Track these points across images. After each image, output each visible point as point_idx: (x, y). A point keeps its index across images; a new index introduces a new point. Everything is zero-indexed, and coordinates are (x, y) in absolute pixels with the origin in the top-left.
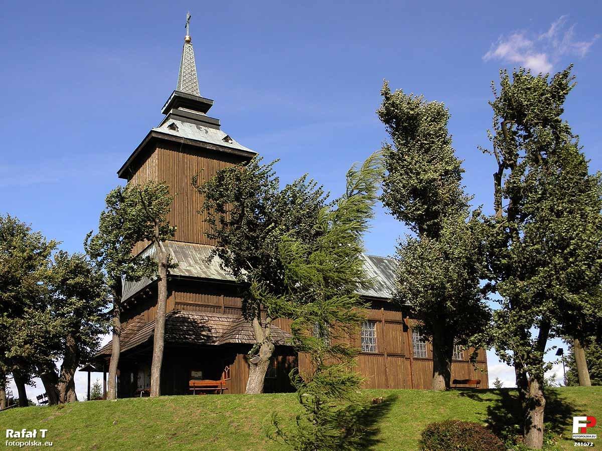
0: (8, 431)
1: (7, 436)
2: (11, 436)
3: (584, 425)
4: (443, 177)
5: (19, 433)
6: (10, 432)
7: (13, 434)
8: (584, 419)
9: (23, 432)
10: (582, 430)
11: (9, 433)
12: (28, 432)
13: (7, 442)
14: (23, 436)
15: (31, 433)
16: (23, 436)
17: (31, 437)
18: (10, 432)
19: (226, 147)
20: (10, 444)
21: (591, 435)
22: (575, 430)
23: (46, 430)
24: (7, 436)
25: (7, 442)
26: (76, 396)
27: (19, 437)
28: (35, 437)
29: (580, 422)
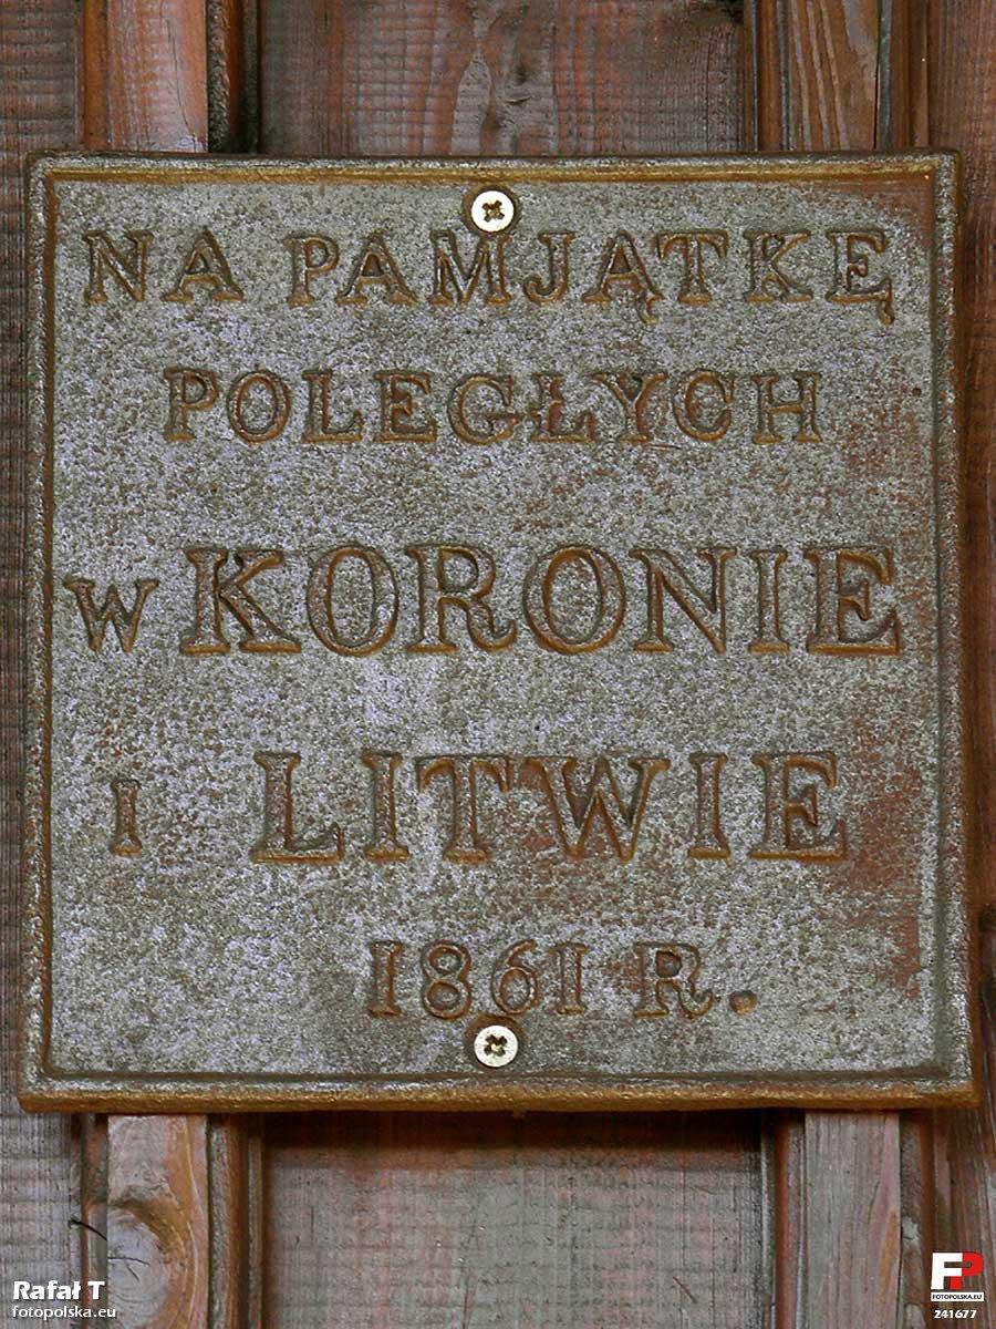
0: (17, 1284)
1: (16, 1297)
2: (25, 1297)
3: (957, 1272)
4: (154, 728)
5: (41, 1289)
6: (22, 1287)
7: (29, 1292)
8: (957, 1257)
9: (51, 1286)
10: (950, 1284)
11: (20, 1289)
12: (61, 1287)
13: (14, 1310)
14: (51, 1297)
15: (67, 1289)
16: (51, 1297)
17: (42, 1297)
18: (22, 1287)
19: (929, 115)
20: (23, 1313)
21: (972, 1294)
22: (937, 1282)
23: (103, 1283)
24: (16, 1297)
25: (14, 1310)
26: (901, 1157)
27: (42, 1297)
28: (76, 1297)
29: (948, 1265)
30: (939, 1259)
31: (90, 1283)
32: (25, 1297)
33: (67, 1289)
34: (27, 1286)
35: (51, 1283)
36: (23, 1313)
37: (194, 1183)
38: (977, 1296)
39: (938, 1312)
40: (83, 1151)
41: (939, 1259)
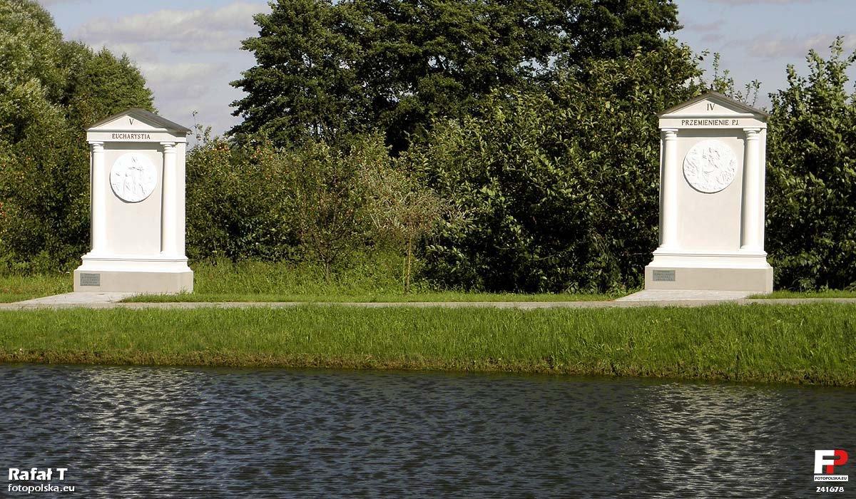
0: (11, 470)
1: (10, 478)
3: (831, 462)
5: (27, 474)
6: (14, 472)
7: (19, 475)
8: (831, 453)
10: (826, 470)
11: (13, 473)
12: (39, 472)
13: (9, 487)
14: (33, 478)
15: (43, 473)
16: (33, 478)
18: (14, 472)
20: (15, 489)
21: (841, 476)
22: (818, 469)
25: (9, 487)
27: (27, 478)
28: (49, 478)
29: (825, 458)
30: (819, 454)
31: (58, 470)
32: (16, 478)
33: (43, 473)
34: (17, 471)
35: (33, 469)
36: (15, 489)
37: (33, 303)
38: (845, 478)
39: (819, 488)
40: (746, 144)
41: (819, 454)
